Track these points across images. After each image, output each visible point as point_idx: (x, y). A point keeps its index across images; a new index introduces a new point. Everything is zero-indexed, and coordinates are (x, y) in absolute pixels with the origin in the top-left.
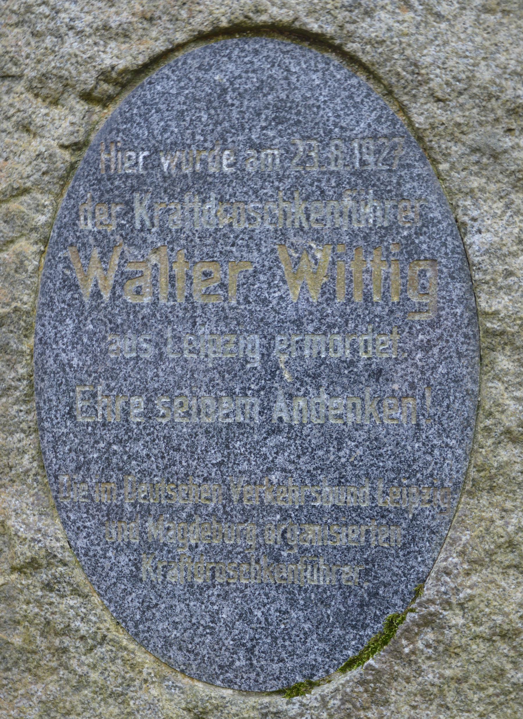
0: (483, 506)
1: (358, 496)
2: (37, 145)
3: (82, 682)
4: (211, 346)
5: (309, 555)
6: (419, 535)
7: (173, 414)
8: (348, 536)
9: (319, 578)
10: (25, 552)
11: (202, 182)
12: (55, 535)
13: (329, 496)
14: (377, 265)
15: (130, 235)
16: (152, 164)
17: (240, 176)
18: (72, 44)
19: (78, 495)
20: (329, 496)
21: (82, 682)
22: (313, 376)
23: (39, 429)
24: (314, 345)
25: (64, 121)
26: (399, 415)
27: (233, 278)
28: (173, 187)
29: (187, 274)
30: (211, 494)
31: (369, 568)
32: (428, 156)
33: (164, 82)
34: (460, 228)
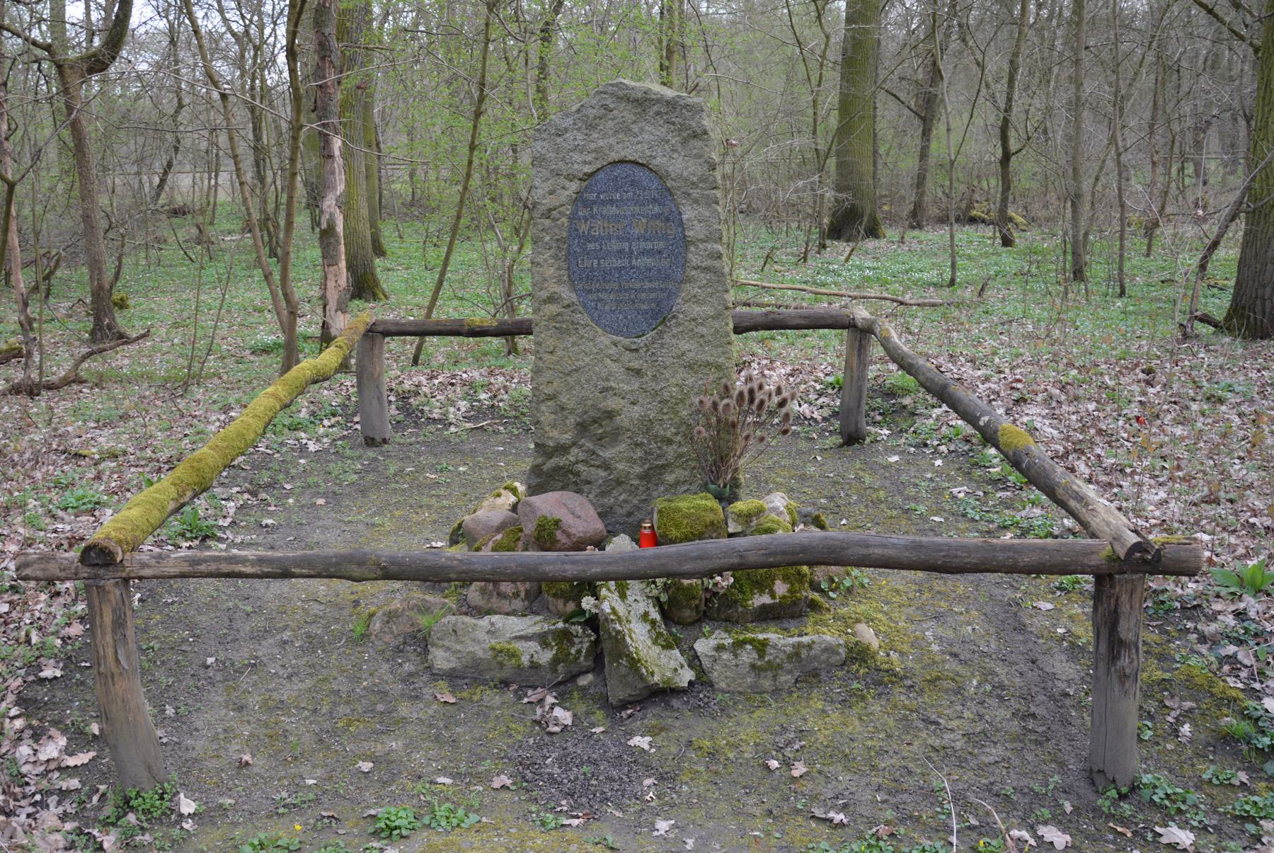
0: (688, 286)
1: (655, 285)
2: (567, 193)
3: (583, 337)
4: (614, 246)
5: (643, 301)
6: (671, 295)
7: (605, 264)
8: (653, 296)
9: (645, 307)
10: (566, 302)
11: (612, 202)
12: (574, 298)
13: (648, 285)
14: (659, 223)
15: (592, 216)
16: (598, 197)
17: (622, 200)
18: (576, 166)
19: (580, 286)
20: (648, 285)
21: (583, 337)
22: (643, 253)
23: (568, 269)
24: (643, 245)
25: (574, 186)
26: (665, 263)
27: (621, 227)
28: (604, 203)
29: (1067, 468)
30: (615, 286)
31: (659, 303)
32: (671, 194)
33: (601, 175)
34: (680, 214)
